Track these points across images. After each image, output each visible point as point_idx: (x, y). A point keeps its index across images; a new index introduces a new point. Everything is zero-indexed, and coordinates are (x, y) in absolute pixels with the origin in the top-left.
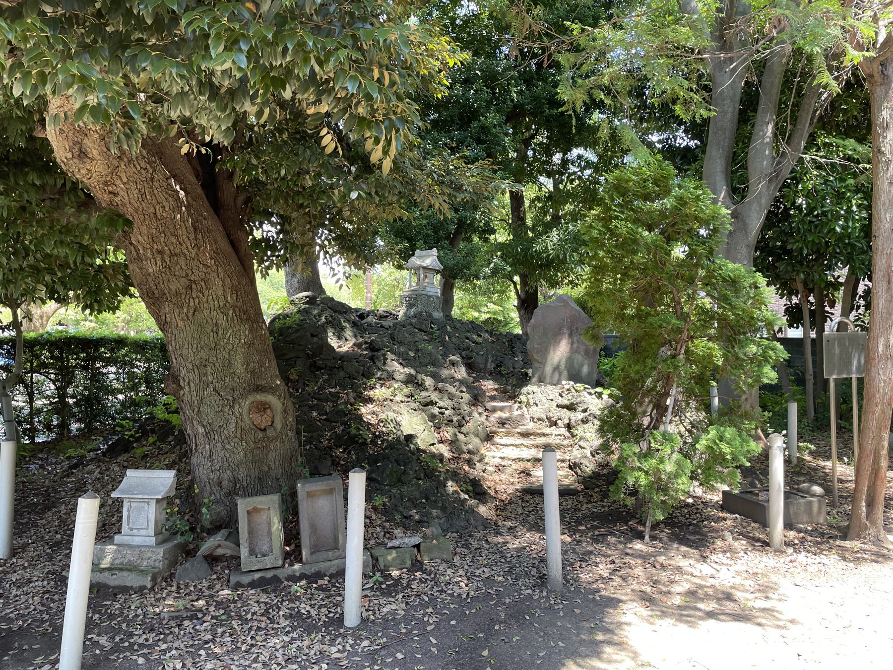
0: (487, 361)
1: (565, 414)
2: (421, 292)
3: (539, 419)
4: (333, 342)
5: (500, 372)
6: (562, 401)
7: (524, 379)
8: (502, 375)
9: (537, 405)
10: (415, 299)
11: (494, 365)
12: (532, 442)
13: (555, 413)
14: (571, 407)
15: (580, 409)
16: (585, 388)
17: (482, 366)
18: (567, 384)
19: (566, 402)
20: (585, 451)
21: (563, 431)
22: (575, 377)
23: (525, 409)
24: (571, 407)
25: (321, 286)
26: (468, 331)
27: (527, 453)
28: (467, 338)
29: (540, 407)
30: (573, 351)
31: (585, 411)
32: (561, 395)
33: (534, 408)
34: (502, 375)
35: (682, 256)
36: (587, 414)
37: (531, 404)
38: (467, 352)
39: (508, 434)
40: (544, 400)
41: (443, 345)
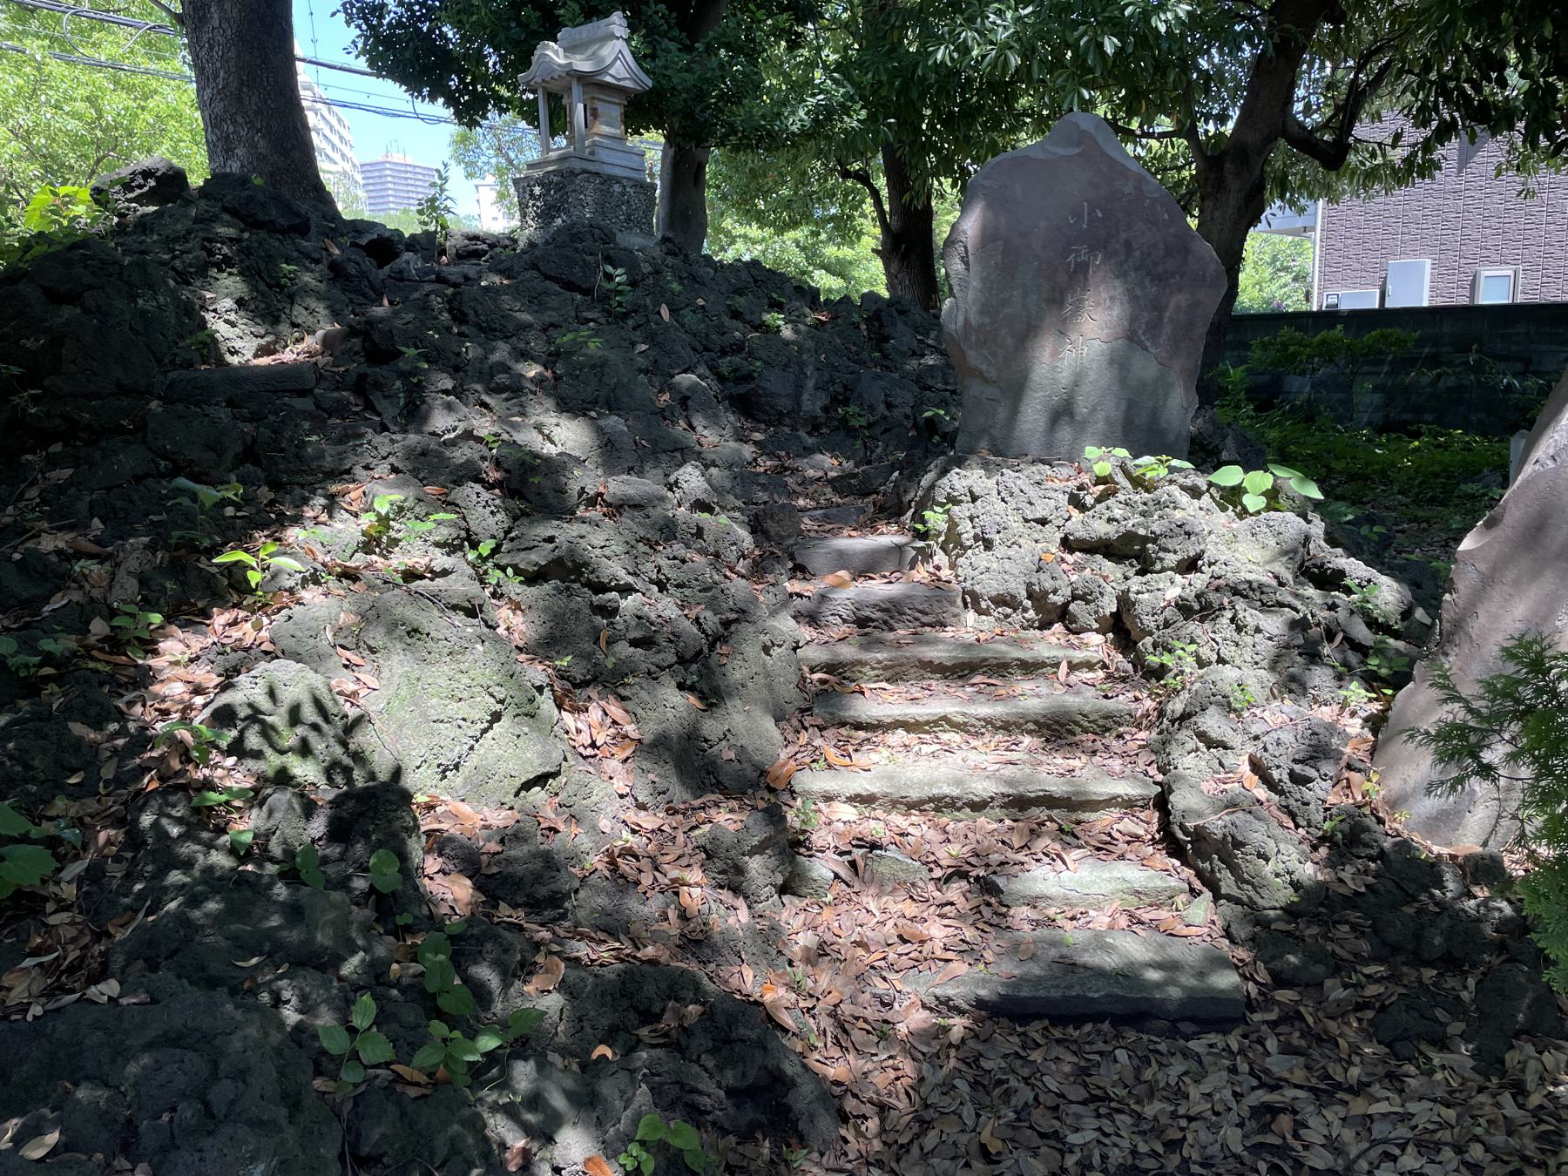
0: (799, 387)
1: (1111, 579)
2: (577, 165)
3: (1000, 601)
4: (238, 339)
5: (844, 421)
6: (1078, 526)
7: (935, 444)
8: (852, 432)
9: (988, 545)
10: (560, 187)
11: (823, 400)
12: (985, 710)
13: (1072, 573)
14: (1130, 550)
15: (1171, 559)
16: (1172, 470)
17: (784, 404)
18: (1103, 459)
19: (1101, 529)
20: (1230, 758)
21: (1096, 644)
22: (1141, 433)
23: (940, 558)
24: (1130, 550)
25: (319, 187)
26: (739, 292)
27: (979, 766)
28: (736, 315)
29: (1000, 551)
30: (1133, 336)
31: (1190, 566)
32: (1076, 502)
33: (980, 557)
34: (852, 432)
35: (276, 891)
36: (1199, 581)
37: (967, 538)
38: (737, 359)
39: (894, 674)
40: (1016, 525)
41: (651, 338)
